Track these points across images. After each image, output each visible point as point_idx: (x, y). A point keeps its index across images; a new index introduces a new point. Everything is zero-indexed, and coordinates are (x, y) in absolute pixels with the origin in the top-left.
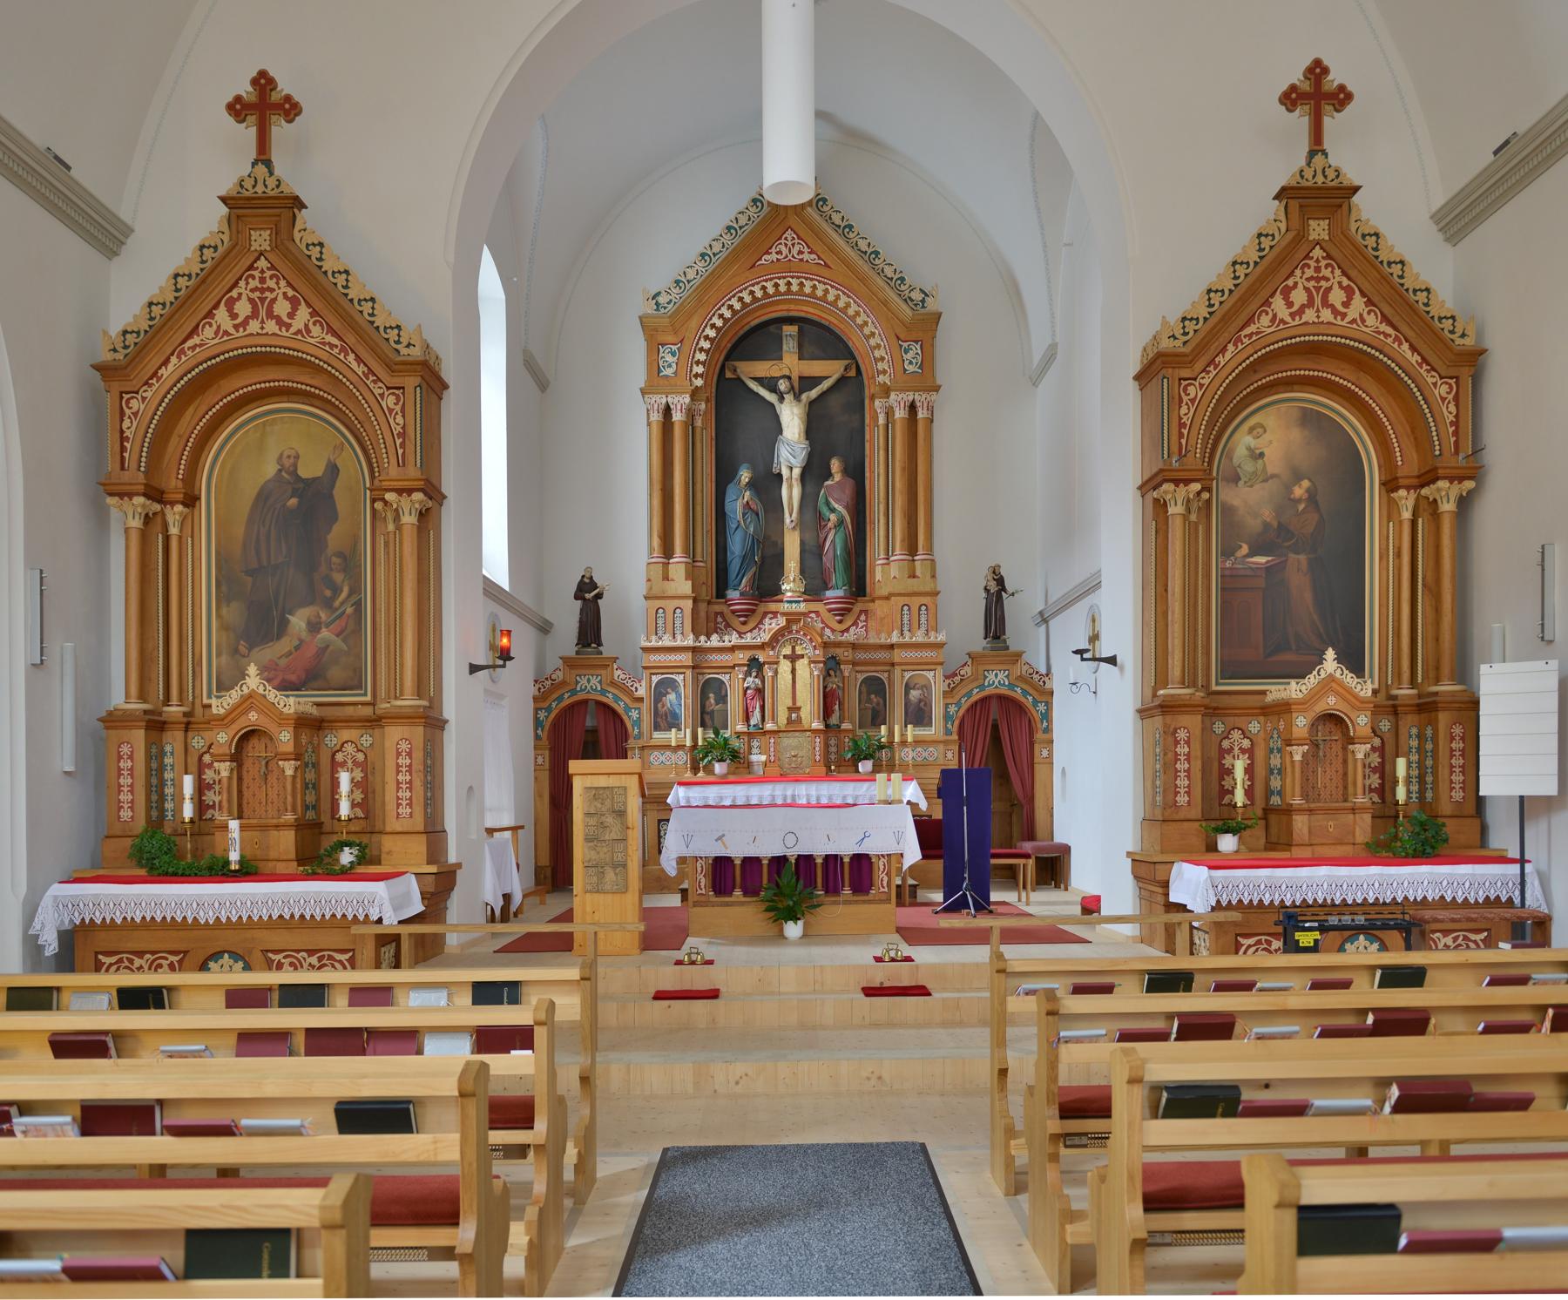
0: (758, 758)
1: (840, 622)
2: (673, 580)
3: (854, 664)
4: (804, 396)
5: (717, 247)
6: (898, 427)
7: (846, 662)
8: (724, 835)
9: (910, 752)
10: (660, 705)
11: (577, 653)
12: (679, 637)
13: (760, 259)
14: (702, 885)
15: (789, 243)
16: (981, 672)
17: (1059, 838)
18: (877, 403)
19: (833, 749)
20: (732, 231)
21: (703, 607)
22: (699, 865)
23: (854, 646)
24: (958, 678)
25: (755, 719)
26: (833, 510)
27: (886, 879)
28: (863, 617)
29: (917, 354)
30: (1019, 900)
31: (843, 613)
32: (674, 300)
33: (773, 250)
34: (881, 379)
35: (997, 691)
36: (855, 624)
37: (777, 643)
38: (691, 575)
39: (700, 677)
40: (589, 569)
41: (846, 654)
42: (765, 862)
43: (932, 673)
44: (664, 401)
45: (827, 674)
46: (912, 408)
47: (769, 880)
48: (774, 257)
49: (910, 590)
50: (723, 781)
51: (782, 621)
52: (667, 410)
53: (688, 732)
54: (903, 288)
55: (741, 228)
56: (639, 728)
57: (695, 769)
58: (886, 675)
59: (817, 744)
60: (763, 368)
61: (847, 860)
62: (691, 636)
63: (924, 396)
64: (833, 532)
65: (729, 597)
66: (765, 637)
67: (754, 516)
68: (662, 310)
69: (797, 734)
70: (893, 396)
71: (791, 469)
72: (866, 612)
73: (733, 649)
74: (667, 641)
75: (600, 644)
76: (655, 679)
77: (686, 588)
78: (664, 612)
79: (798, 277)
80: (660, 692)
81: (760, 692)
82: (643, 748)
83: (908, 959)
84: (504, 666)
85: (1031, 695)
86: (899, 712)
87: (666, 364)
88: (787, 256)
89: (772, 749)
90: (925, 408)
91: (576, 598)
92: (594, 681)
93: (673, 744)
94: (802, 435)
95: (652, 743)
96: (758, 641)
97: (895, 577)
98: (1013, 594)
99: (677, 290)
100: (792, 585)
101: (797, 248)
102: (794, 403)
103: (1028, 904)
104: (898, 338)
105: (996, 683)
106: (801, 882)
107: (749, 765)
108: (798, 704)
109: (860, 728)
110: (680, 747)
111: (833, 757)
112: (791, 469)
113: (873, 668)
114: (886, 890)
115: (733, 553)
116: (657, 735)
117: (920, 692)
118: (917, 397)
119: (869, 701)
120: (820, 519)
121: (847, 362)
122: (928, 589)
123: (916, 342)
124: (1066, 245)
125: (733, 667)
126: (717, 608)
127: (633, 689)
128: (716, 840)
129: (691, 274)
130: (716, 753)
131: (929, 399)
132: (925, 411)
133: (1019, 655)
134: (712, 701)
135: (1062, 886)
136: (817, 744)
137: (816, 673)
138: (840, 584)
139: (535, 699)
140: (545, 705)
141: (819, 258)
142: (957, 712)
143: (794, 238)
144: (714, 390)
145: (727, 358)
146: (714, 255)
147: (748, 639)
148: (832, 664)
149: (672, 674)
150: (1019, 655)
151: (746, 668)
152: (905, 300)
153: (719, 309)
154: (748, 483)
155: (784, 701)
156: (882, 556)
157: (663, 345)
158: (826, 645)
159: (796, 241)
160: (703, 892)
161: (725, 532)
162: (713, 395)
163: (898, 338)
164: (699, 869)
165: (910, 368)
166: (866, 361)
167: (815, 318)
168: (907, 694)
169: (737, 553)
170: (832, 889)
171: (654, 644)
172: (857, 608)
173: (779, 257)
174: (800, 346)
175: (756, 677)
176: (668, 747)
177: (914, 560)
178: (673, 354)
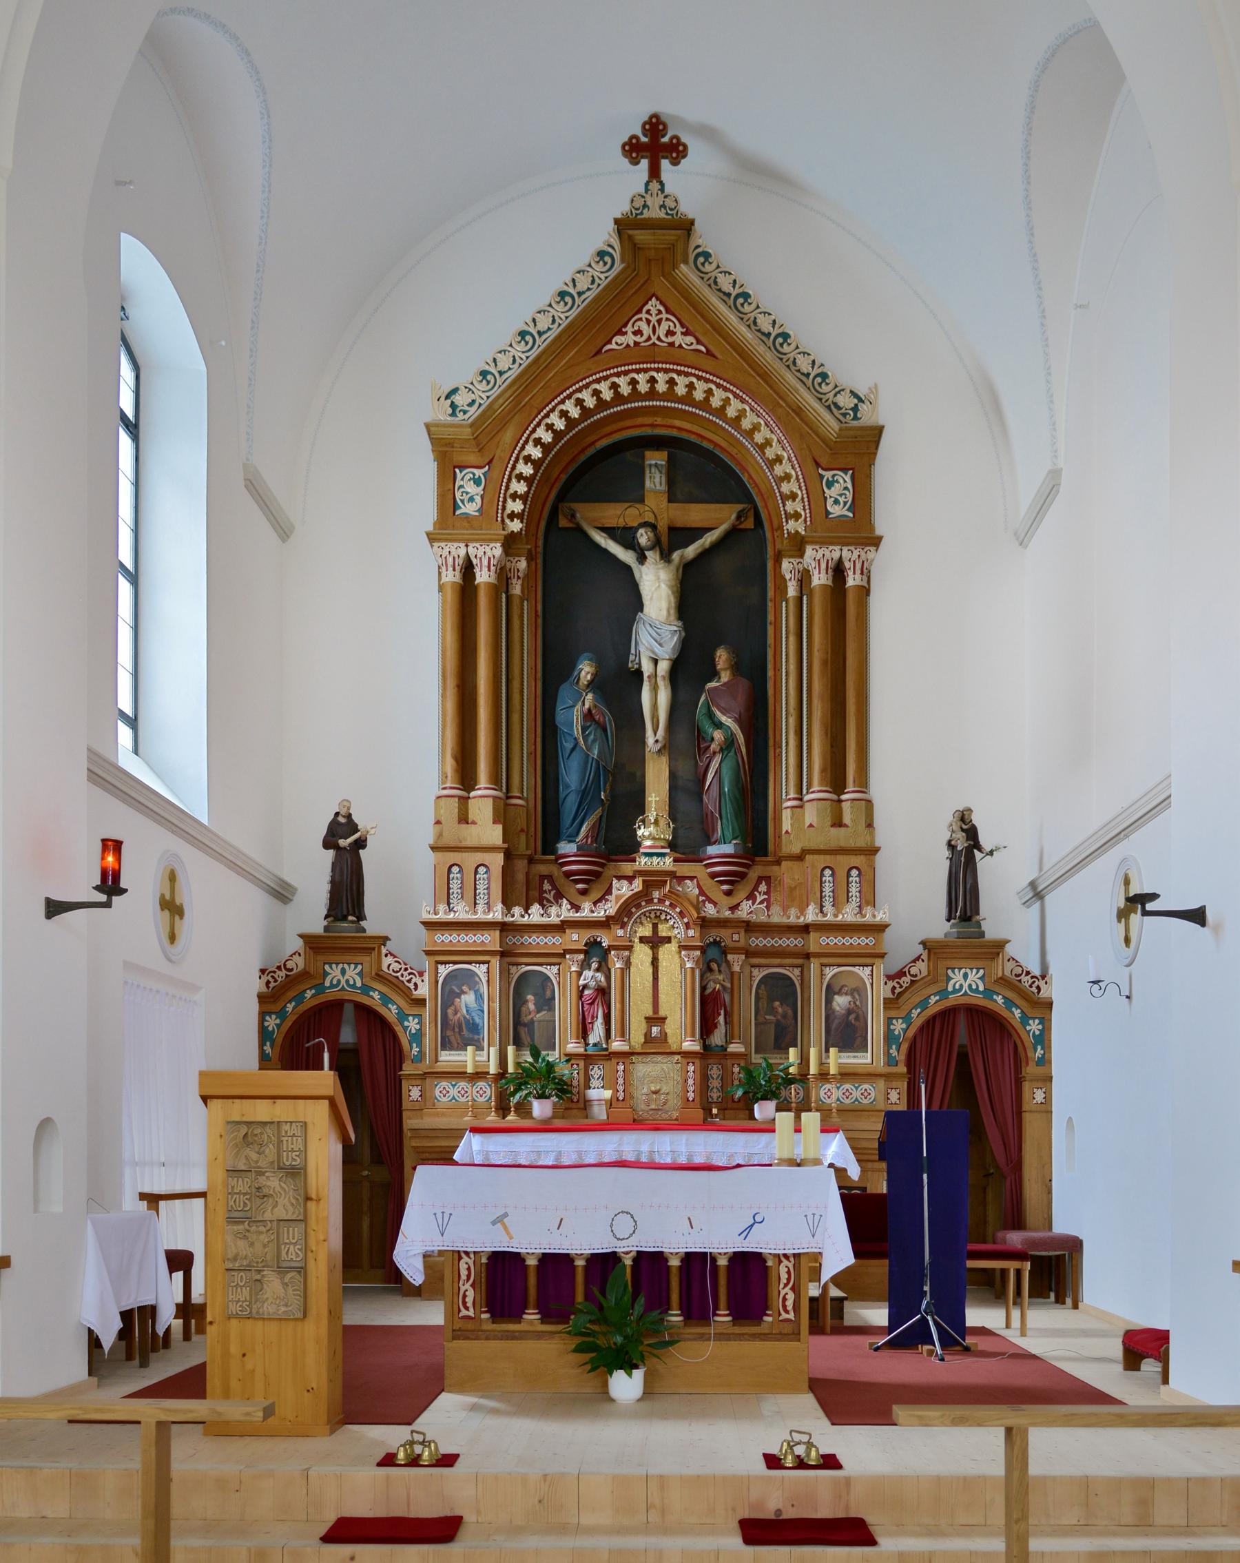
0: (599, 1094)
1: (728, 893)
2: (474, 823)
3: (749, 953)
4: (676, 556)
5: (544, 323)
6: (817, 600)
7: (736, 951)
8: (506, 1215)
9: (834, 1090)
10: (450, 1011)
11: (326, 929)
12: (480, 908)
13: (609, 342)
14: (469, 1300)
15: (654, 319)
16: (941, 971)
17: (1062, 1226)
18: (786, 565)
19: (715, 1083)
20: (568, 299)
21: (521, 865)
22: (463, 1267)
23: (749, 927)
24: (906, 980)
25: (596, 1035)
26: (719, 725)
27: (791, 1297)
28: (763, 887)
29: (846, 488)
30: (1008, 1326)
31: (734, 879)
32: (479, 401)
33: (629, 329)
34: (791, 526)
35: (966, 1000)
36: (751, 897)
37: (630, 917)
38: (502, 814)
39: (513, 969)
40: (346, 803)
41: (736, 937)
42: (580, 1263)
43: (868, 970)
44: (462, 552)
45: (706, 968)
46: (838, 571)
47: (588, 1296)
48: (630, 339)
49: (833, 844)
50: (545, 1127)
51: (638, 885)
52: (468, 569)
53: (494, 1051)
54: (825, 388)
55: (580, 294)
56: (420, 1045)
57: (503, 1109)
58: (797, 971)
59: (691, 1074)
60: (615, 514)
61: (723, 1262)
62: (499, 907)
63: (856, 553)
64: (718, 758)
65: (561, 852)
66: (610, 908)
67: (599, 731)
68: (460, 416)
69: (659, 1058)
70: (809, 551)
71: (656, 662)
72: (768, 879)
73: (562, 927)
74: (462, 912)
75: (361, 917)
76: (444, 970)
77: (494, 834)
78: (461, 871)
79: (666, 371)
80: (451, 991)
81: (603, 993)
82: (425, 1075)
83: (830, 1462)
84: (107, 905)
85: (1017, 1007)
86: (816, 1028)
87: (466, 497)
88: (649, 338)
89: (621, 1081)
90: (858, 571)
91: (327, 844)
92: (352, 973)
93: (470, 1070)
94: (672, 612)
95: (440, 1067)
96: (600, 913)
97: (811, 826)
98: (991, 853)
99: (483, 386)
100: (652, 828)
101: (665, 326)
102: (662, 564)
103: (1023, 1334)
104: (818, 465)
105: (965, 987)
106: (641, 1300)
107: (586, 1104)
108: (662, 1013)
109: (756, 1052)
110: (479, 1075)
111: (715, 1095)
112: (656, 662)
113: (777, 961)
114: (791, 1316)
115: (567, 786)
116: (445, 1056)
117: (849, 998)
118: (846, 554)
119: (773, 1011)
120: (700, 741)
121: (740, 507)
122: (861, 843)
123: (845, 470)
124: (1077, 307)
125: (563, 955)
126: (543, 869)
127: (411, 986)
128: (494, 1223)
129: (504, 363)
130: (533, 1087)
131: (863, 557)
132: (858, 576)
133: (999, 946)
134: (531, 1006)
135: (1069, 1301)
136: (691, 1074)
137: (689, 965)
138: (729, 835)
139: (262, 998)
140: (277, 1007)
141: (699, 342)
142: (905, 1031)
143: (660, 312)
144: (540, 543)
145: (562, 497)
146: (540, 334)
147: (586, 911)
148: (713, 953)
149: (470, 963)
150: (999, 946)
151: (582, 956)
152: (829, 407)
153: (547, 416)
154: (590, 683)
155: (640, 1008)
156: (792, 795)
157: (462, 468)
158: (705, 924)
159: (664, 316)
160: (471, 1313)
161: (557, 757)
162: (540, 550)
163: (818, 465)
164: (464, 1273)
165: (836, 511)
166: (770, 505)
167: (693, 438)
168: (829, 1001)
169: (573, 787)
170: (697, 1312)
171: (442, 916)
172: (754, 874)
173: (638, 339)
174: (671, 482)
175: (598, 970)
176: (459, 1075)
177: (840, 801)
178: (477, 482)
